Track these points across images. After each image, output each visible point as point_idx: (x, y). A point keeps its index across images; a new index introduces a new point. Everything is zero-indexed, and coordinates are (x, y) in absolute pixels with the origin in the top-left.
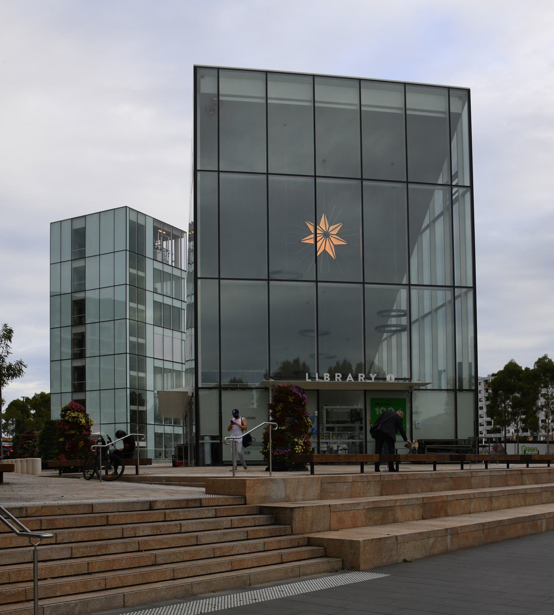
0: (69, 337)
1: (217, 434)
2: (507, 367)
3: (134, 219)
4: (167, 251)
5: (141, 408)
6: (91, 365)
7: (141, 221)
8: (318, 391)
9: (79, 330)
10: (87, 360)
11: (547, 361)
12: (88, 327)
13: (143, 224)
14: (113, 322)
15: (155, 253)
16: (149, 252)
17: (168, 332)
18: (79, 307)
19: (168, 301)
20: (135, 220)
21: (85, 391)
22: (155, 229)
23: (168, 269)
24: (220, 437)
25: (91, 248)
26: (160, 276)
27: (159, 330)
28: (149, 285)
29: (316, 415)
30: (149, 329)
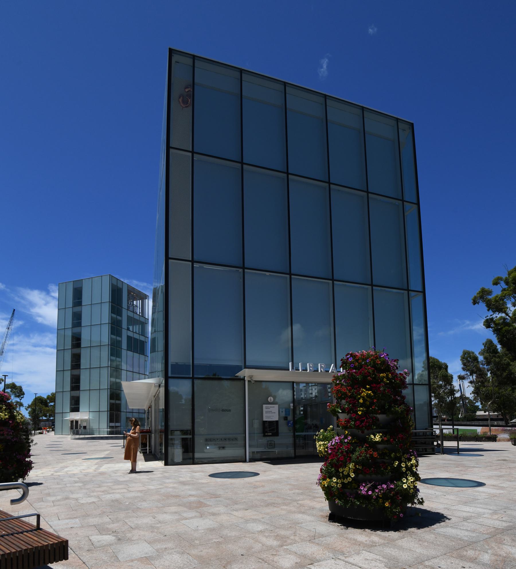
0: (71, 334)
1: (189, 427)
3: (115, 283)
4: (137, 306)
6: (85, 312)
7: (120, 285)
12: (83, 308)
13: (121, 287)
15: (128, 307)
17: (136, 355)
18: (77, 341)
19: (136, 336)
21: (80, 369)
22: (129, 292)
23: (136, 317)
24: (192, 432)
25: (85, 300)
26: (131, 321)
27: (130, 353)
28: (124, 325)
29: (292, 407)
30: (124, 353)
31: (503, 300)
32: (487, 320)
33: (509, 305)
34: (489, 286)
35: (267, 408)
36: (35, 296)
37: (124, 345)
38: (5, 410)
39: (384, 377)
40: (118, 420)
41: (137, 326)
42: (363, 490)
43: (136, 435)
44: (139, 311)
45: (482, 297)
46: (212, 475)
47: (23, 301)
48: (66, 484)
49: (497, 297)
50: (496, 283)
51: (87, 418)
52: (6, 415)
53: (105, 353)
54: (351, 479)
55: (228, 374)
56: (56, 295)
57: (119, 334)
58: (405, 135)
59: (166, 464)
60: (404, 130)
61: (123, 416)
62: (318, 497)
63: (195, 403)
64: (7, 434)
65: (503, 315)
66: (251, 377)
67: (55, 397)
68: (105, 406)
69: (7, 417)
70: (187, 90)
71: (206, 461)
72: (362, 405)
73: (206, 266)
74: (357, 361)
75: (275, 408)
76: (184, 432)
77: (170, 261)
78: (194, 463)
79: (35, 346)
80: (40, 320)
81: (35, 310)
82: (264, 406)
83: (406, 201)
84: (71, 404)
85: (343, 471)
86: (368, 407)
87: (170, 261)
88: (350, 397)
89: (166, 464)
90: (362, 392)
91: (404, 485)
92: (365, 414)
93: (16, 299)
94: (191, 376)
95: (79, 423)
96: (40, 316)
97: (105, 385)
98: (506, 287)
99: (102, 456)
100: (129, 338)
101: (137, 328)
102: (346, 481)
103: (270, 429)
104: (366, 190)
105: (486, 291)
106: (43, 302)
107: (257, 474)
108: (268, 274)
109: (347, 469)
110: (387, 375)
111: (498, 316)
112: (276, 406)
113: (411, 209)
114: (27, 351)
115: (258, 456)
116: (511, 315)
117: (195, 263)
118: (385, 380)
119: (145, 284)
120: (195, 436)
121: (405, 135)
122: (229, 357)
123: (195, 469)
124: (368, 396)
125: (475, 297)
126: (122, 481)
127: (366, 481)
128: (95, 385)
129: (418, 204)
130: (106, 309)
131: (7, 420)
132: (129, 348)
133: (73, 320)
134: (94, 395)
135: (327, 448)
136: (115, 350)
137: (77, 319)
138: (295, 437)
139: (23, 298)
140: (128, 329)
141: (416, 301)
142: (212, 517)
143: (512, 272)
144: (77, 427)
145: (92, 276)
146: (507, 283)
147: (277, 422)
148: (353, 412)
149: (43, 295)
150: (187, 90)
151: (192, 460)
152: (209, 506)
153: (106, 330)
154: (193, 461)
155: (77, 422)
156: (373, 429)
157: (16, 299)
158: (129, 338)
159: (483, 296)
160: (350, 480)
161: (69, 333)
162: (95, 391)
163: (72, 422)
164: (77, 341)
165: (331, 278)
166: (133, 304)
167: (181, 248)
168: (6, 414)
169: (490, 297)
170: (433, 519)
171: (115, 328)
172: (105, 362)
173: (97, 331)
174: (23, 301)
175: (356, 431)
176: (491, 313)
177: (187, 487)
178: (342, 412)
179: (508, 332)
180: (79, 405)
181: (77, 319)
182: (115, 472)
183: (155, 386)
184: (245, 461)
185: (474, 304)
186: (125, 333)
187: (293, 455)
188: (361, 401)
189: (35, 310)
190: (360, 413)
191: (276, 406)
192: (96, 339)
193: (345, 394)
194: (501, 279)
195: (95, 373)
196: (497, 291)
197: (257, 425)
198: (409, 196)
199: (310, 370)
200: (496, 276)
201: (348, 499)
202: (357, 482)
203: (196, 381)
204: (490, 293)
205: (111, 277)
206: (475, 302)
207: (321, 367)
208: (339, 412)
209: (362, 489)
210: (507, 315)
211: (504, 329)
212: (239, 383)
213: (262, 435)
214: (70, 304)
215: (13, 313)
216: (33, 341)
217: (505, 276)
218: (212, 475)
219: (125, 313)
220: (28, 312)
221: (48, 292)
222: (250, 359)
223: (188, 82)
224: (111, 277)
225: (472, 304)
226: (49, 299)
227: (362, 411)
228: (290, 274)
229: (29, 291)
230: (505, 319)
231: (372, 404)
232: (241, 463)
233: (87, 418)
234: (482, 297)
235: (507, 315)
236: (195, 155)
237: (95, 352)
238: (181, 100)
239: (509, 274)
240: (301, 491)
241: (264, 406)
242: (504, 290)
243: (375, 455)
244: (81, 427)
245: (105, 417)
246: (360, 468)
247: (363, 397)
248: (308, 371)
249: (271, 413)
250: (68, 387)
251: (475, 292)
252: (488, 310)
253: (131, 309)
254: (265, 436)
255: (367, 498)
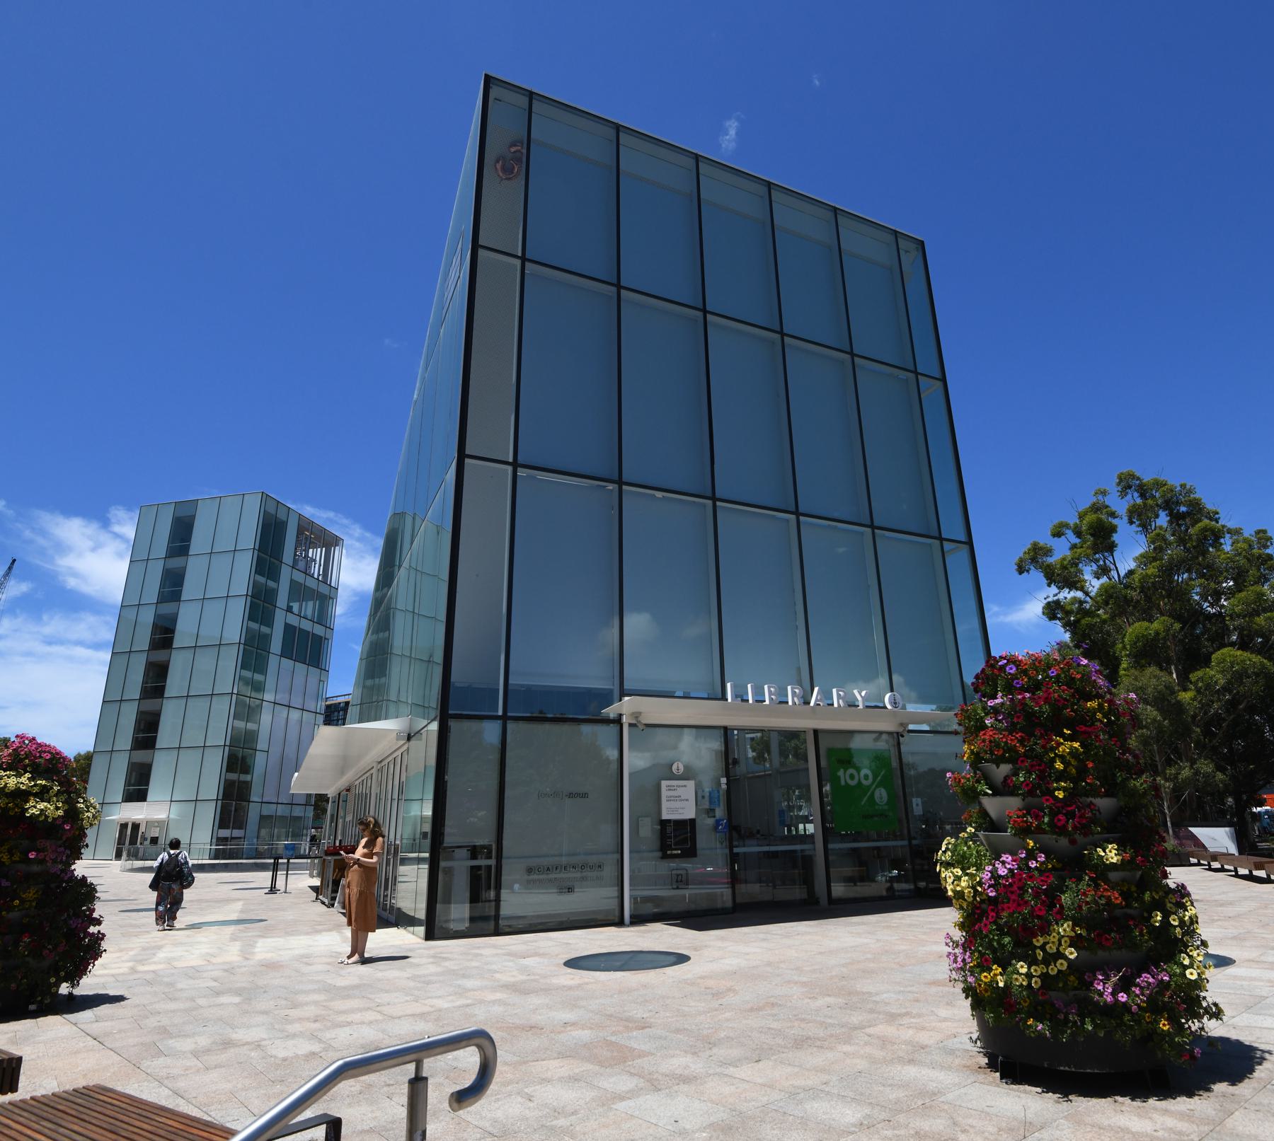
2: (932, 771)
5: (243, 777)
6: (195, 569)
7: (282, 515)
8: (725, 728)
9: (150, 705)
10: (174, 652)
11: (93, 929)
14: (176, 752)
16: (288, 556)
18: (164, 636)
19: (306, 625)
20: (273, 512)
22: (300, 531)
23: (311, 583)
25: (199, 542)
26: (299, 592)
27: (287, 663)
28: (282, 600)
29: (724, 786)
30: (273, 661)
31: (1077, 565)
32: (1049, 603)
33: (1088, 576)
34: (1046, 539)
35: (670, 788)
36: (73, 530)
37: (276, 645)
38: (58, 794)
39: (1094, 711)
40: (240, 824)
41: (311, 604)
42: (1105, 989)
43: (375, 859)
44: (316, 570)
45: (1034, 560)
46: (573, 963)
47: (41, 541)
48: (193, 999)
49: (1064, 559)
50: (1057, 534)
51: (162, 816)
52: (57, 808)
53: (230, 660)
54: (1066, 964)
55: (582, 709)
56: (129, 531)
57: (267, 620)
58: (910, 259)
59: (429, 936)
60: (908, 252)
61: (253, 813)
62: (314, 991)
63: (507, 779)
64: (54, 861)
65: (1079, 594)
66: (637, 715)
67: (89, 766)
68: (211, 789)
69: (60, 813)
70: (513, 150)
71: (520, 924)
72: (1061, 776)
73: (542, 476)
74: (1025, 672)
75: (688, 790)
76: (474, 852)
77: (467, 461)
78: (497, 932)
79: (50, 641)
80: (72, 583)
81: (65, 562)
82: (664, 783)
83: (921, 375)
84: (128, 783)
85: (1045, 944)
86: (1076, 780)
87: (467, 461)
88: (1025, 755)
89: (429, 936)
90: (1059, 744)
91: (1187, 972)
92: (1072, 795)
93: (28, 534)
94: (500, 713)
95: (142, 829)
96: (75, 574)
97: (219, 736)
98: (1077, 541)
99: (234, 917)
100: (288, 628)
101: (310, 608)
102: (1053, 971)
103: (676, 839)
104: (848, 350)
105: (1041, 549)
106: (91, 544)
107: (682, 959)
108: (659, 494)
109: (1053, 938)
110: (1100, 705)
111: (1067, 595)
112: (691, 784)
113: (930, 389)
114: (29, 654)
115: (650, 909)
116: (1092, 594)
117: (519, 469)
118: (1099, 716)
119: (331, 514)
120: (504, 861)
121: (910, 259)
122: (586, 673)
123: (513, 948)
124: (1073, 753)
125: (1021, 560)
126: (345, 988)
127: (1106, 968)
128: (193, 737)
129: (943, 380)
130: (245, 563)
131: (59, 822)
132: (286, 653)
133: (162, 585)
134: (190, 760)
135: (980, 883)
136: (254, 654)
137: (172, 585)
138: (734, 858)
139: (43, 533)
140: (289, 609)
141: (957, 560)
142: (684, 1088)
143: (1086, 513)
144: (133, 841)
145: (216, 493)
146: (1078, 534)
147: (692, 821)
148: (1043, 794)
149: (92, 529)
150: (513, 150)
151: (492, 924)
152: (642, 1055)
153: (238, 610)
154: (488, 923)
155: (136, 827)
156: (1093, 834)
157: (28, 534)
158: (288, 628)
159: (1035, 558)
160: (1062, 965)
161: (148, 617)
162: (190, 751)
163: (124, 826)
164: (164, 636)
165: (793, 508)
166: (307, 556)
167: (493, 435)
168: (60, 805)
169: (1050, 560)
170: (1236, 1061)
171: (260, 605)
172: (226, 683)
173: (215, 611)
174: (41, 541)
175: (1048, 839)
176: (1054, 589)
177: (535, 1000)
178: (994, 795)
179: (1091, 627)
180: (147, 784)
181: (172, 585)
182: (306, 959)
183: (398, 737)
184: (620, 923)
185: (1020, 573)
186: (280, 619)
187: (729, 904)
188: (1059, 765)
189: (65, 562)
190: (1060, 795)
191: (691, 784)
192: (210, 633)
193: (1012, 749)
194: (1067, 526)
195: (198, 708)
196: (1061, 550)
197: (648, 830)
198: (926, 363)
199: (771, 699)
200: (1056, 522)
201: (1061, 1016)
202: (1082, 973)
203: (511, 726)
204: (1048, 552)
205: (265, 497)
206: (1021, 569)
207: (794, 694)
208: (986, 794)
209: (1100, 987)
210: (1087, 594)
211: (1083, 622)
212: (613, 729)
213: (659, 854)
214: (161, 549)
215: (10, 568)
216: (48, 630)
217: (1073, 520)
218: (573, 963)
219: (285, 573)
220: (48, 566)
221: (105, 523)
222: (632, 677)
223: (516, 135)
224: (265, 497)
225: (1016, 573)
226: (104, 537)
227: (1064, 789)
228: (714, 499)
229: (60, 519)
230: (1081, 602)
231: (1083, 772)
232: (658, 926)
233: (163, 816)
234: (1034, 560)
235: (1087, 594)
236: (527, 264)
237: (205, 661)
238: (499, 166)
239: (1081, 517)
240: (459, 982)
241: (664, 783)
242: (1074, 547)
243: (1116, 897)
244: (144, 839)
245: (208, 814)
246: (1084, 933)
247: (1062, 758)
248: (767, 702)
249: (680, 803)
250: (125, 741)
251: (1020, 550)
252: (1049, 585)
253: (301, 565)
254: (665, 857)
255: (1115, 1010)
